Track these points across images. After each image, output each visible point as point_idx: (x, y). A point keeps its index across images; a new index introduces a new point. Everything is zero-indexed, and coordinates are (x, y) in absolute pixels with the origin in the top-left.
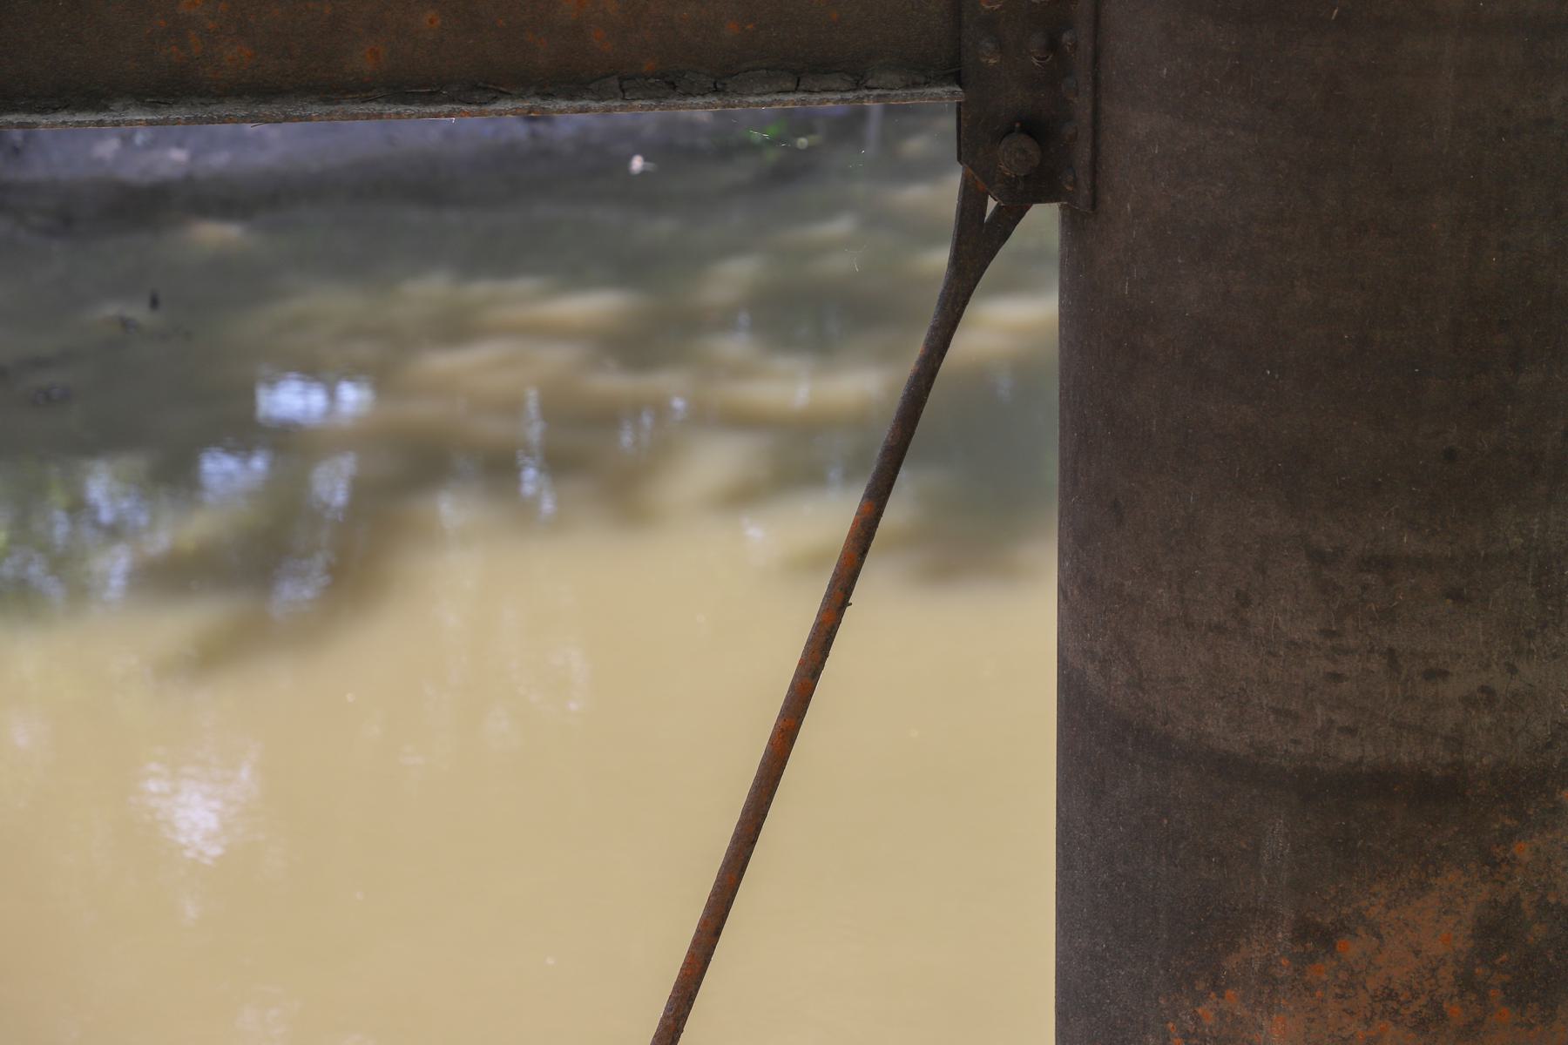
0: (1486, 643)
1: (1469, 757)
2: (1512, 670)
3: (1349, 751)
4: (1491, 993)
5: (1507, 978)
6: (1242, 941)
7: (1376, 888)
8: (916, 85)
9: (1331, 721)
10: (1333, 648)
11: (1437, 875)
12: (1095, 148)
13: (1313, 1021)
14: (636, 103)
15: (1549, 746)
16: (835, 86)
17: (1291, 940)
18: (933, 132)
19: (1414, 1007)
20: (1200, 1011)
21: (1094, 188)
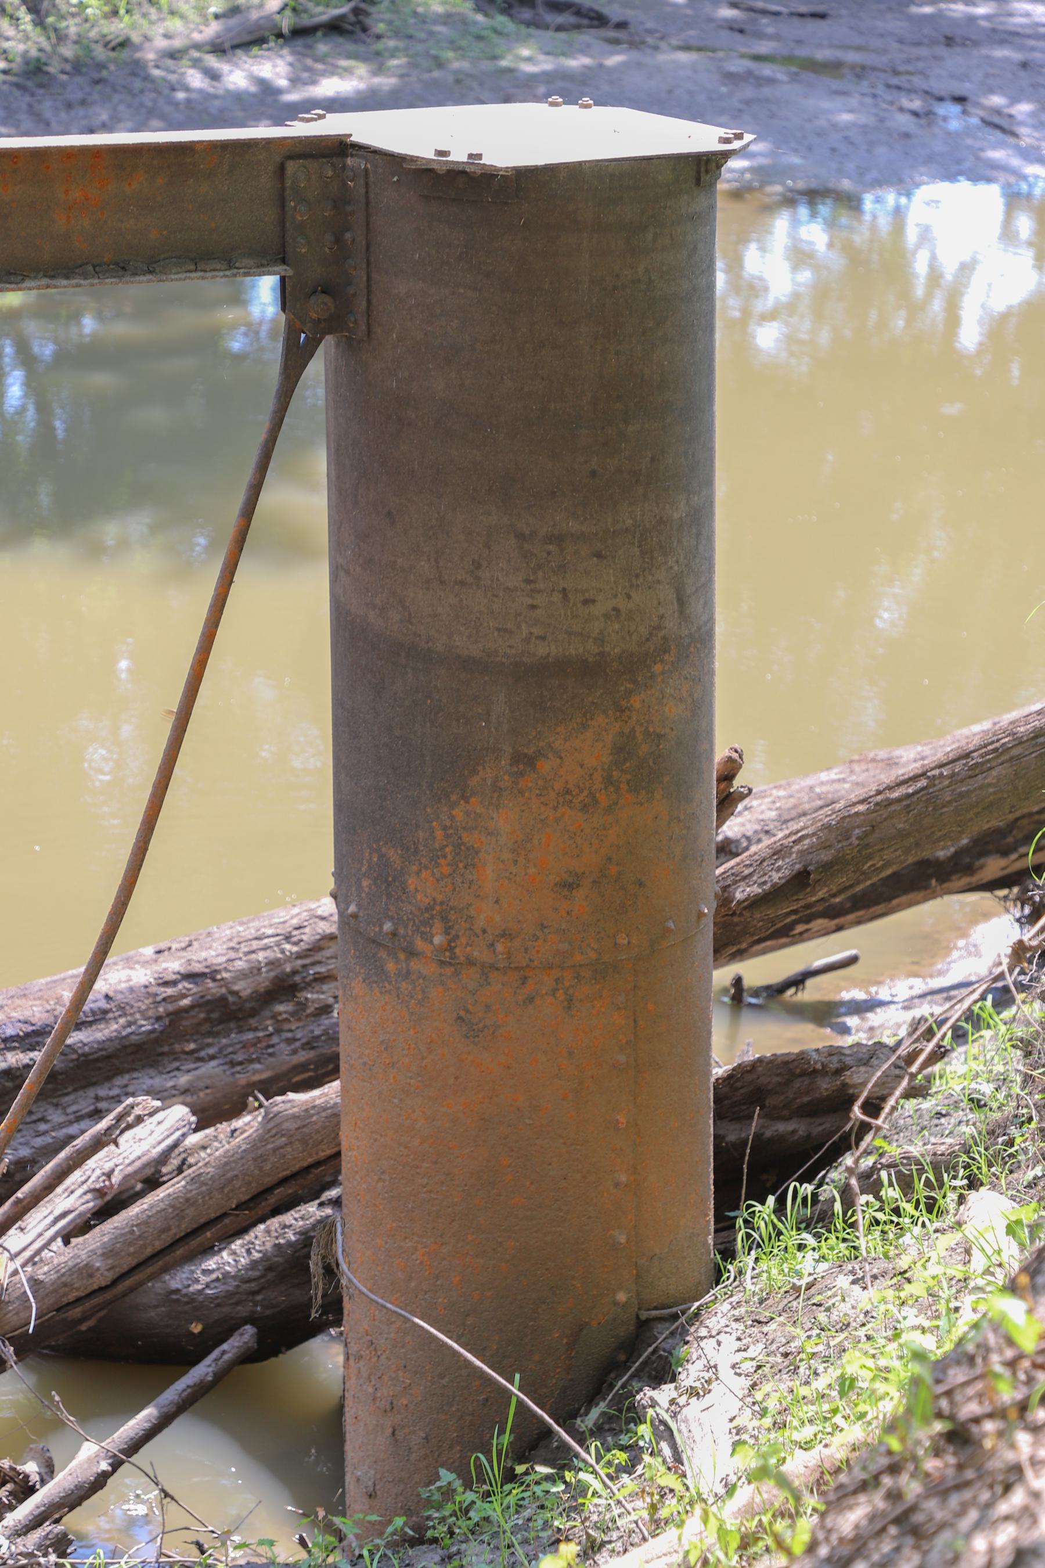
0: (615, 582)
1: (607, 649)
2: (629, 597)
3: (542, 650)
4: (622, 786)
5: (629, 777)
6: (480, 768)
7: (558, 729)
8: (263, 266)
9: (531, 633)
10: (531, 590)
11: (592, 719)
13: (523, 811)
14: (107, 280)
15: (648, 640)
17: (510, 765)
19: (581, 798)
20: (454, 813)
21: (369, 325)
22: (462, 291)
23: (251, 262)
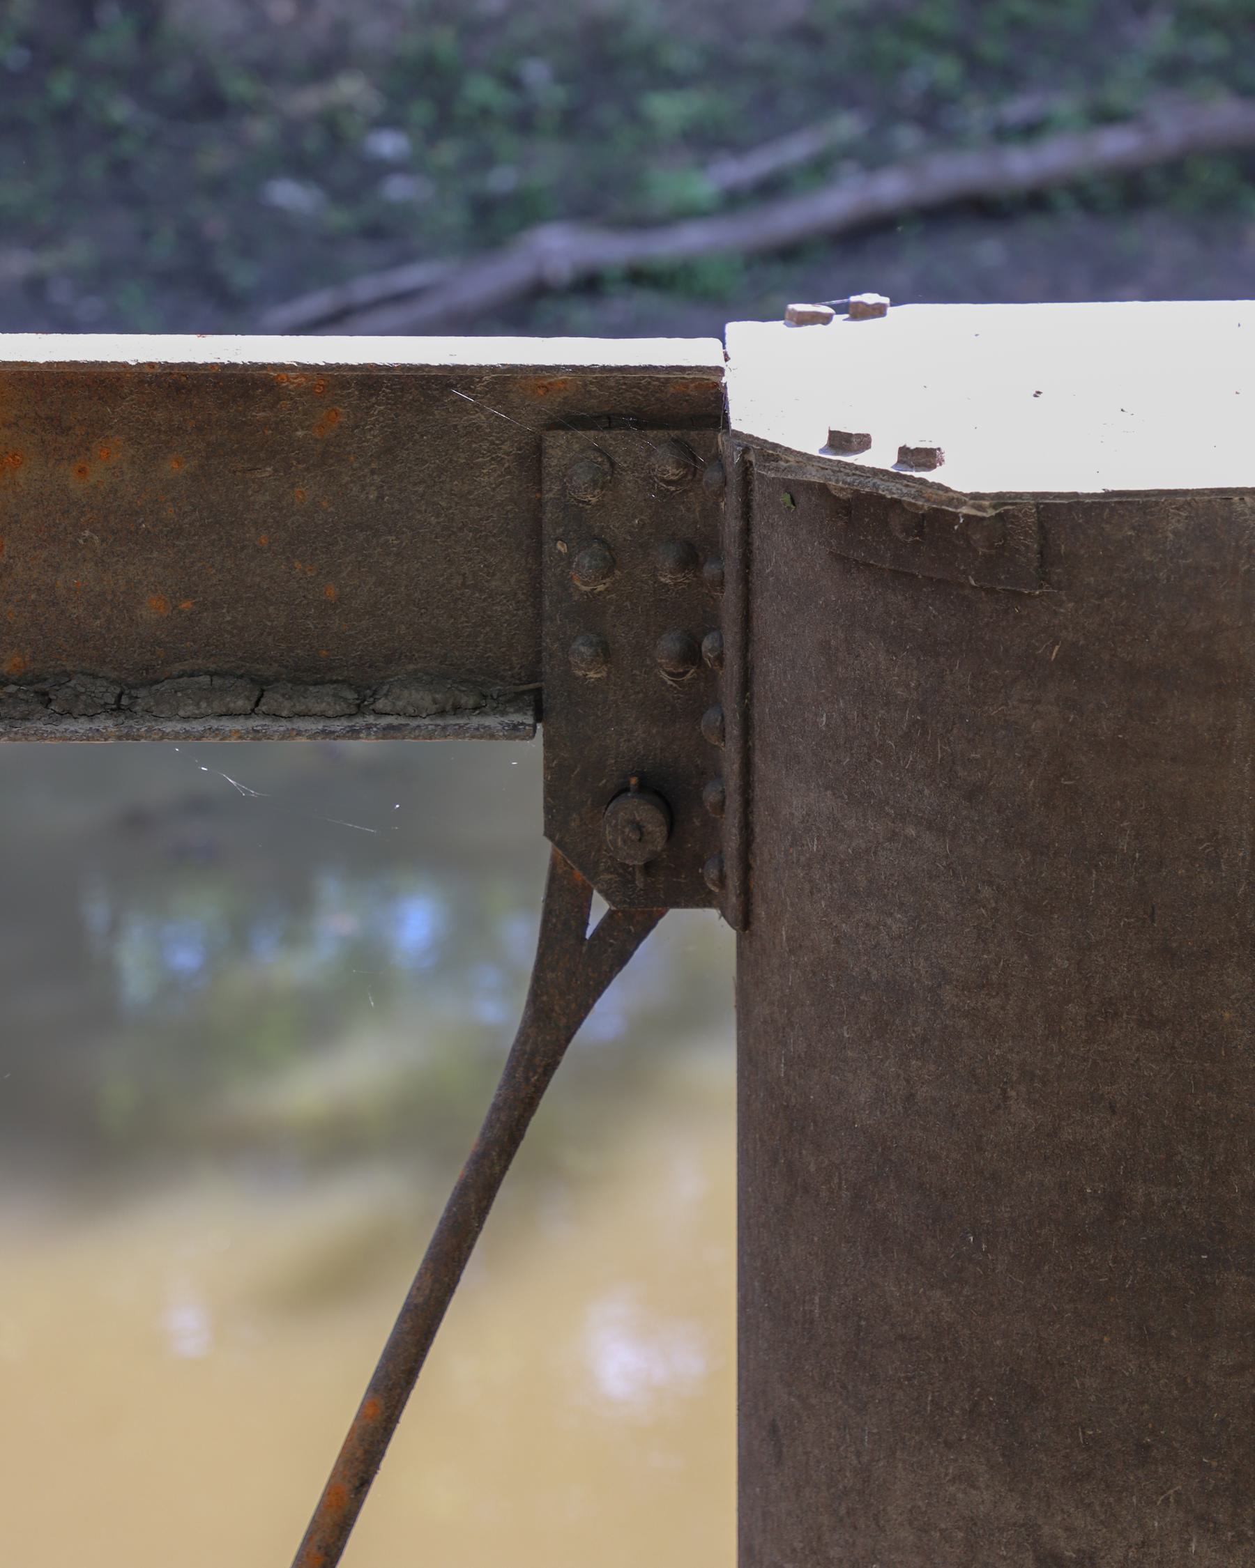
8: (457, 710)
12: (747, 828)
16: (318, 708)
18: (507, 772)
22: (911, 831)
23: (422, 697)
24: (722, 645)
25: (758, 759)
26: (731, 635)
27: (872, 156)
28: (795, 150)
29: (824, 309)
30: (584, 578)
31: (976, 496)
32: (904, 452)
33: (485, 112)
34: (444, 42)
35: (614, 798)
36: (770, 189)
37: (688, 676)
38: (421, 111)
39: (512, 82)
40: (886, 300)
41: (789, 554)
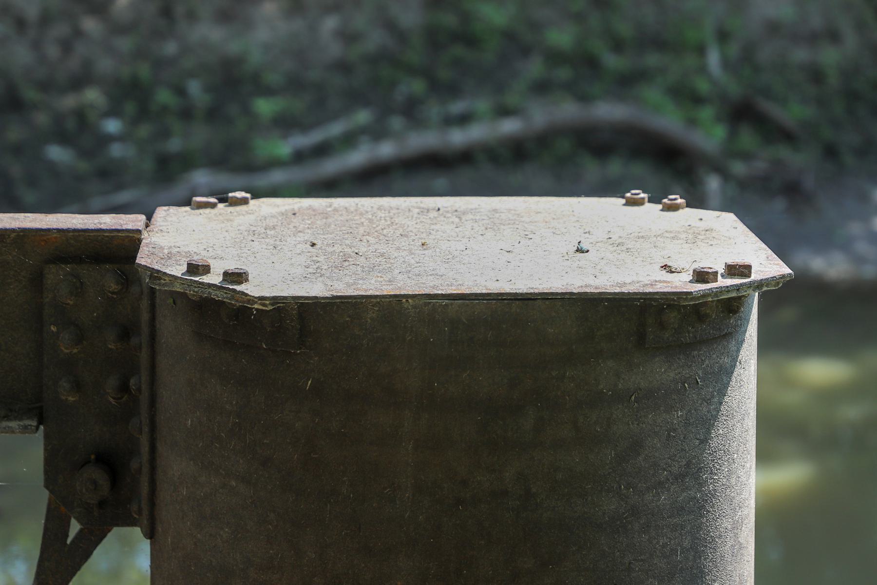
12: (153, 482)
24: (140, 382)
25: (161, 448)
26: (144, 376)
27: (377, 133)
28: (335, 129)
29: (213, 200)
30: (66, 347)
31: (262, 298)
32: (226, 274)
33: (165, 109)
34: (144, 71)
35: (83, 466)
36: (322, 150)
37: (124, 399)
38: (130, 108)
39: (181, 92)
40: (248, 195)
41: (173, 330)
